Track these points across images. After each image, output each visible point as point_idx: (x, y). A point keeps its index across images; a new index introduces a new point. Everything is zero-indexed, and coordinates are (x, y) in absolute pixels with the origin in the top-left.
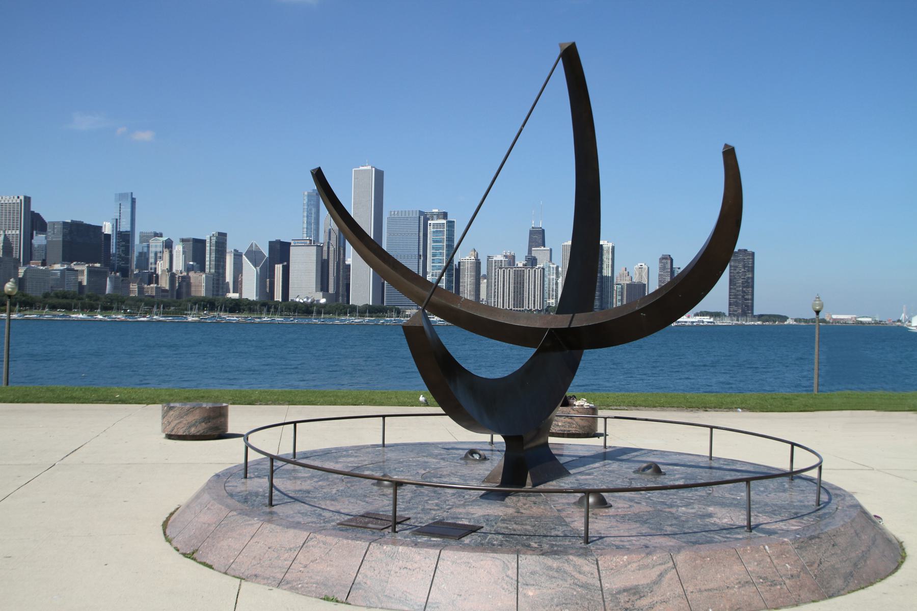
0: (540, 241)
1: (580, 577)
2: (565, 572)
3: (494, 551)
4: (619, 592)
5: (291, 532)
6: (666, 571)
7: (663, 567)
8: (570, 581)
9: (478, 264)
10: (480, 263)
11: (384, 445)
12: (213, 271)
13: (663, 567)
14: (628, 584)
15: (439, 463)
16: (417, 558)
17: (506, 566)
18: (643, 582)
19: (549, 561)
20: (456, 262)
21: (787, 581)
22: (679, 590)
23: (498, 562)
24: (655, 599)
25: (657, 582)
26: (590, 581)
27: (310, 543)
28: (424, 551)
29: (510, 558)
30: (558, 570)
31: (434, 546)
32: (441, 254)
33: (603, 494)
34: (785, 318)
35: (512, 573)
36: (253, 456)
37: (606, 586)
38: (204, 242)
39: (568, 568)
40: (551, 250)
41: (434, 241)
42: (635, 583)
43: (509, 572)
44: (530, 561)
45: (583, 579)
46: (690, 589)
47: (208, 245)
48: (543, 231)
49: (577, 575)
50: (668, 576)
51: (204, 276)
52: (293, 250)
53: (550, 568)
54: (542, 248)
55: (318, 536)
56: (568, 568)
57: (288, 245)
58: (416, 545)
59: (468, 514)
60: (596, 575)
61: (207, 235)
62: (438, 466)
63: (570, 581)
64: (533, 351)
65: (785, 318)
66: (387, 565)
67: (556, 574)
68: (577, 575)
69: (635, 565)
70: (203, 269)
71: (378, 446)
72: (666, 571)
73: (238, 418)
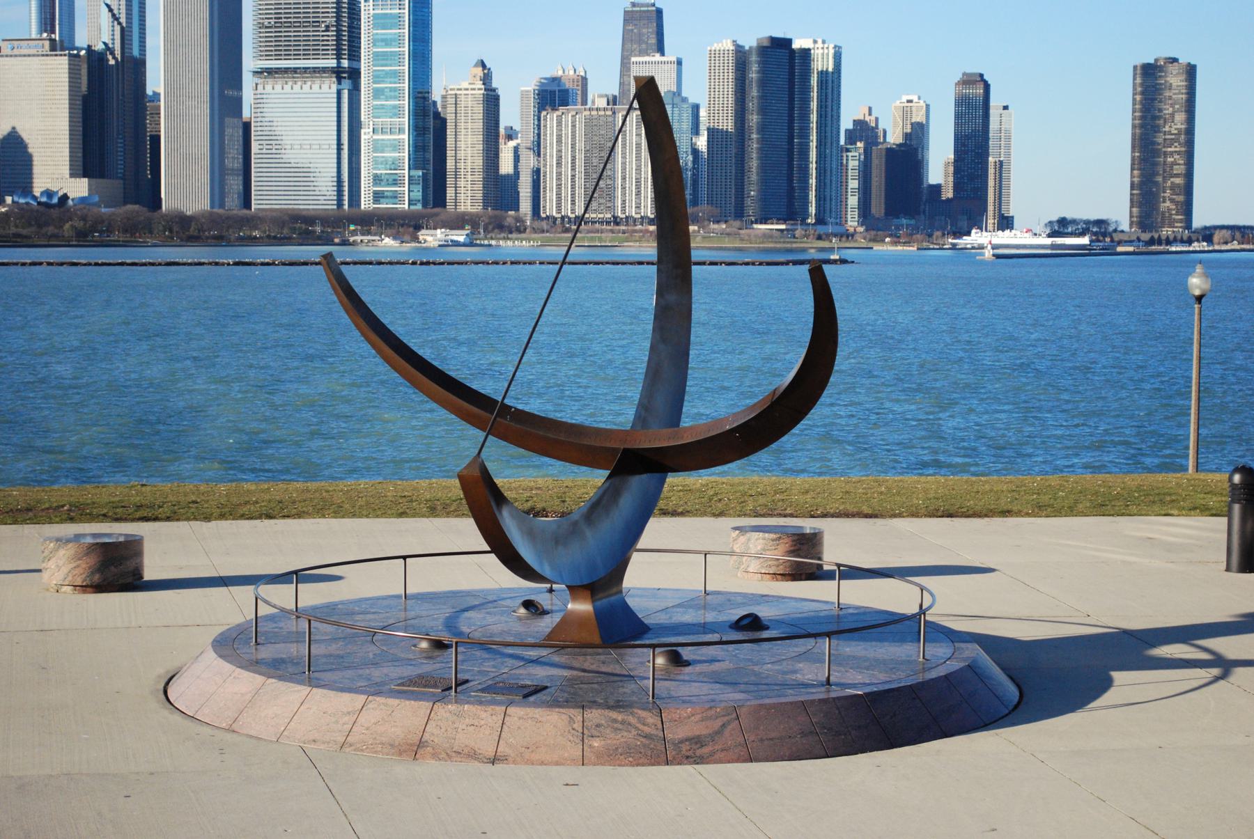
0: (653, 41)
1: (646, 729)
2: (629, 724)
3: (560, 707)
4: (681, 742)
5: (347, 697)
6: (729, 722)
7: (725, 719)
8: (634, 732)
9: (491, 101)
10: (497, 98)
11: (828, 682)
13: (725, 719)
14: (690, 734)
15: (484, 618)
16: (484, 715)
18: (705, 732)
20: (436, 95)
21: (853, 732)
22: (741, 739)
23: (564, 717)
24: (716, 747)
25: (719, 732)
26: (654, 732)
27: (370, 706)
29: (576, 713)
30: (623, 722)
31: (499, 703)
32: (396, 75)
33: (680, 649)
35: (578, 726)
36: (264, 610)
37: (669, 736)
40: (679, 63)
42: (698, 733)
43: (575, 726)
44: (594, 715)
45: (646, 729)
46: (752, 738)
48: (659, 12)
49: (641, 727)
50: (730, 727)
53: (615, 721)
54: (658, 57)
55: (378, 699)
58: (481, 703)
59: (529, 674)
60: (660, 726)
62: (484, 623)
63: (634, 732)
64: (607, 473)
66: (453, 723)
67: (620, 726)
68: (641, 727)
69: (698, 717)
71: (399, 597)
72: (729, 722)
73: (165, 548)
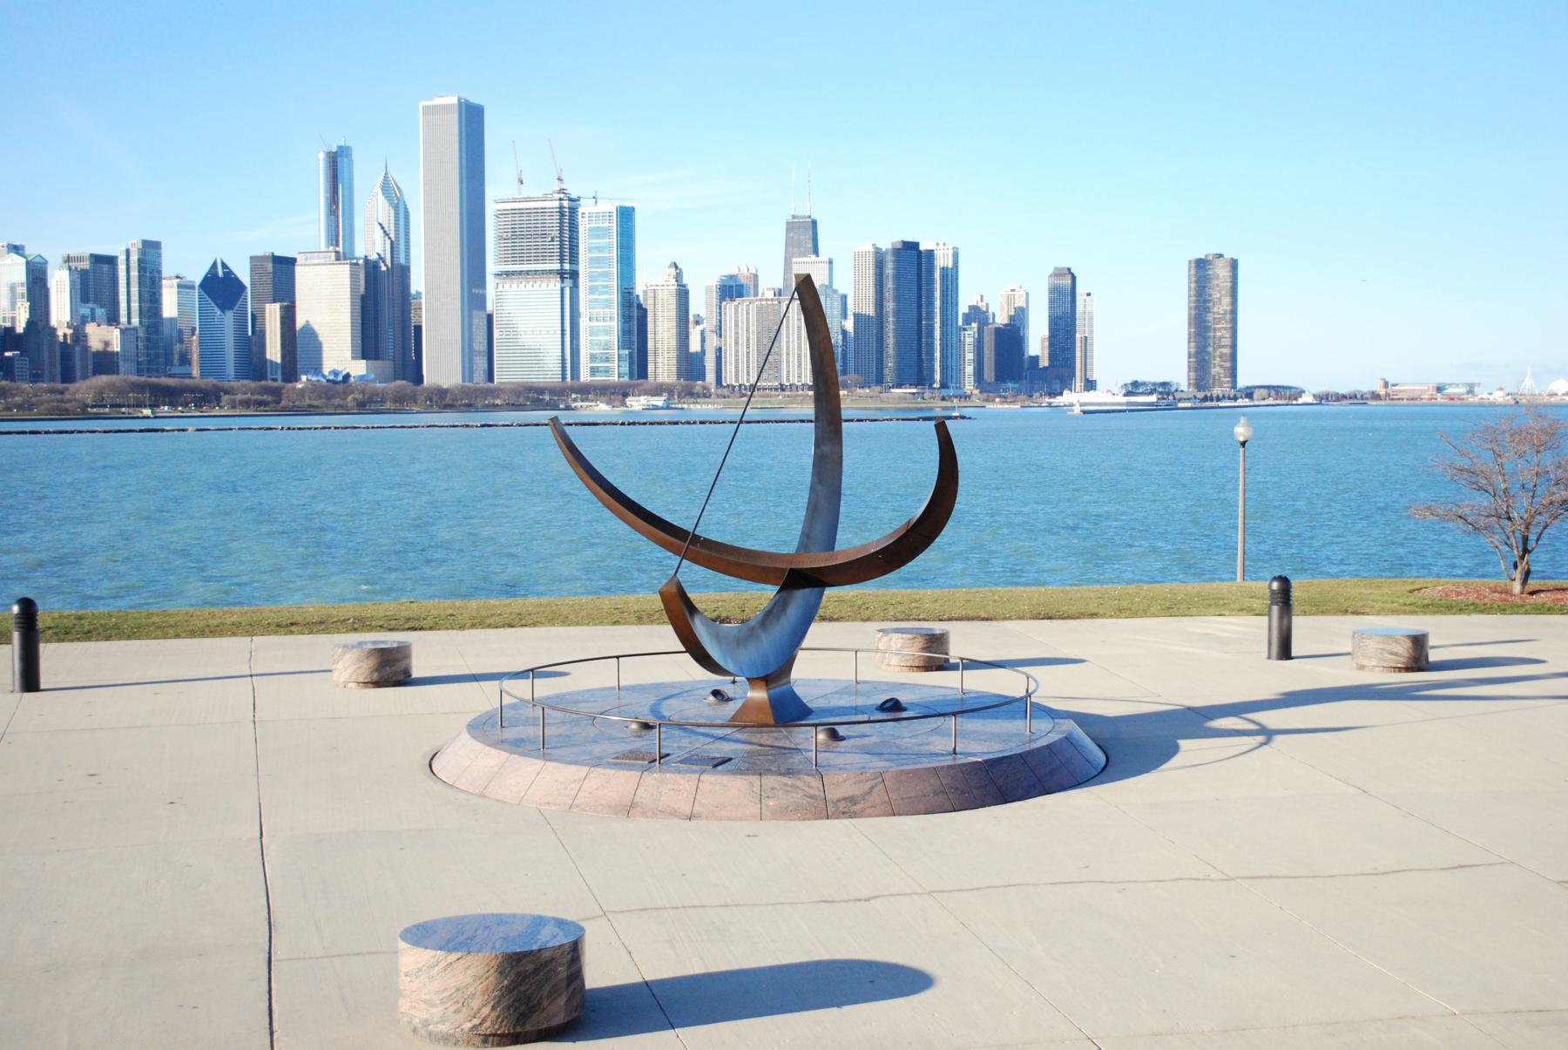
5: (573, 768)
9: (683, 295)
12: (135, 321)
17: (751, 785)
18: (857, 793)
19: (785, 780)
25: (869, 793)
28: (687, 776)
29: (755, 779)
31: (694, 772)
34: (1301, 393)
36: (507, 700)
37: (829, 796)
38: (111, 261)
39: (798, 783)
40: (831, 262)
41: (590, 237)
44: (770, 781)
45: (812, 792)
47: (122, 267)
48: (814, 223)
51: (117, 332)
52: (300, 272)
56: (798, 783)
57: (291, 262)
58: (680, 772)
61: (119, 243)
65: (1301, 393)
70: (113, 319)
